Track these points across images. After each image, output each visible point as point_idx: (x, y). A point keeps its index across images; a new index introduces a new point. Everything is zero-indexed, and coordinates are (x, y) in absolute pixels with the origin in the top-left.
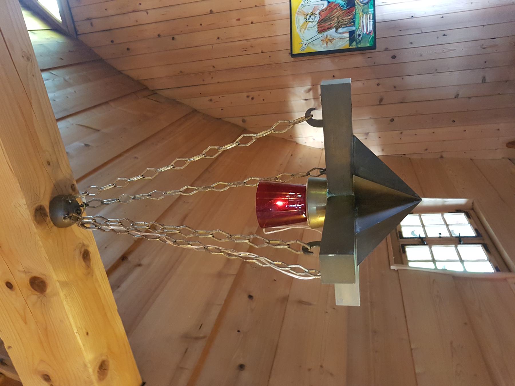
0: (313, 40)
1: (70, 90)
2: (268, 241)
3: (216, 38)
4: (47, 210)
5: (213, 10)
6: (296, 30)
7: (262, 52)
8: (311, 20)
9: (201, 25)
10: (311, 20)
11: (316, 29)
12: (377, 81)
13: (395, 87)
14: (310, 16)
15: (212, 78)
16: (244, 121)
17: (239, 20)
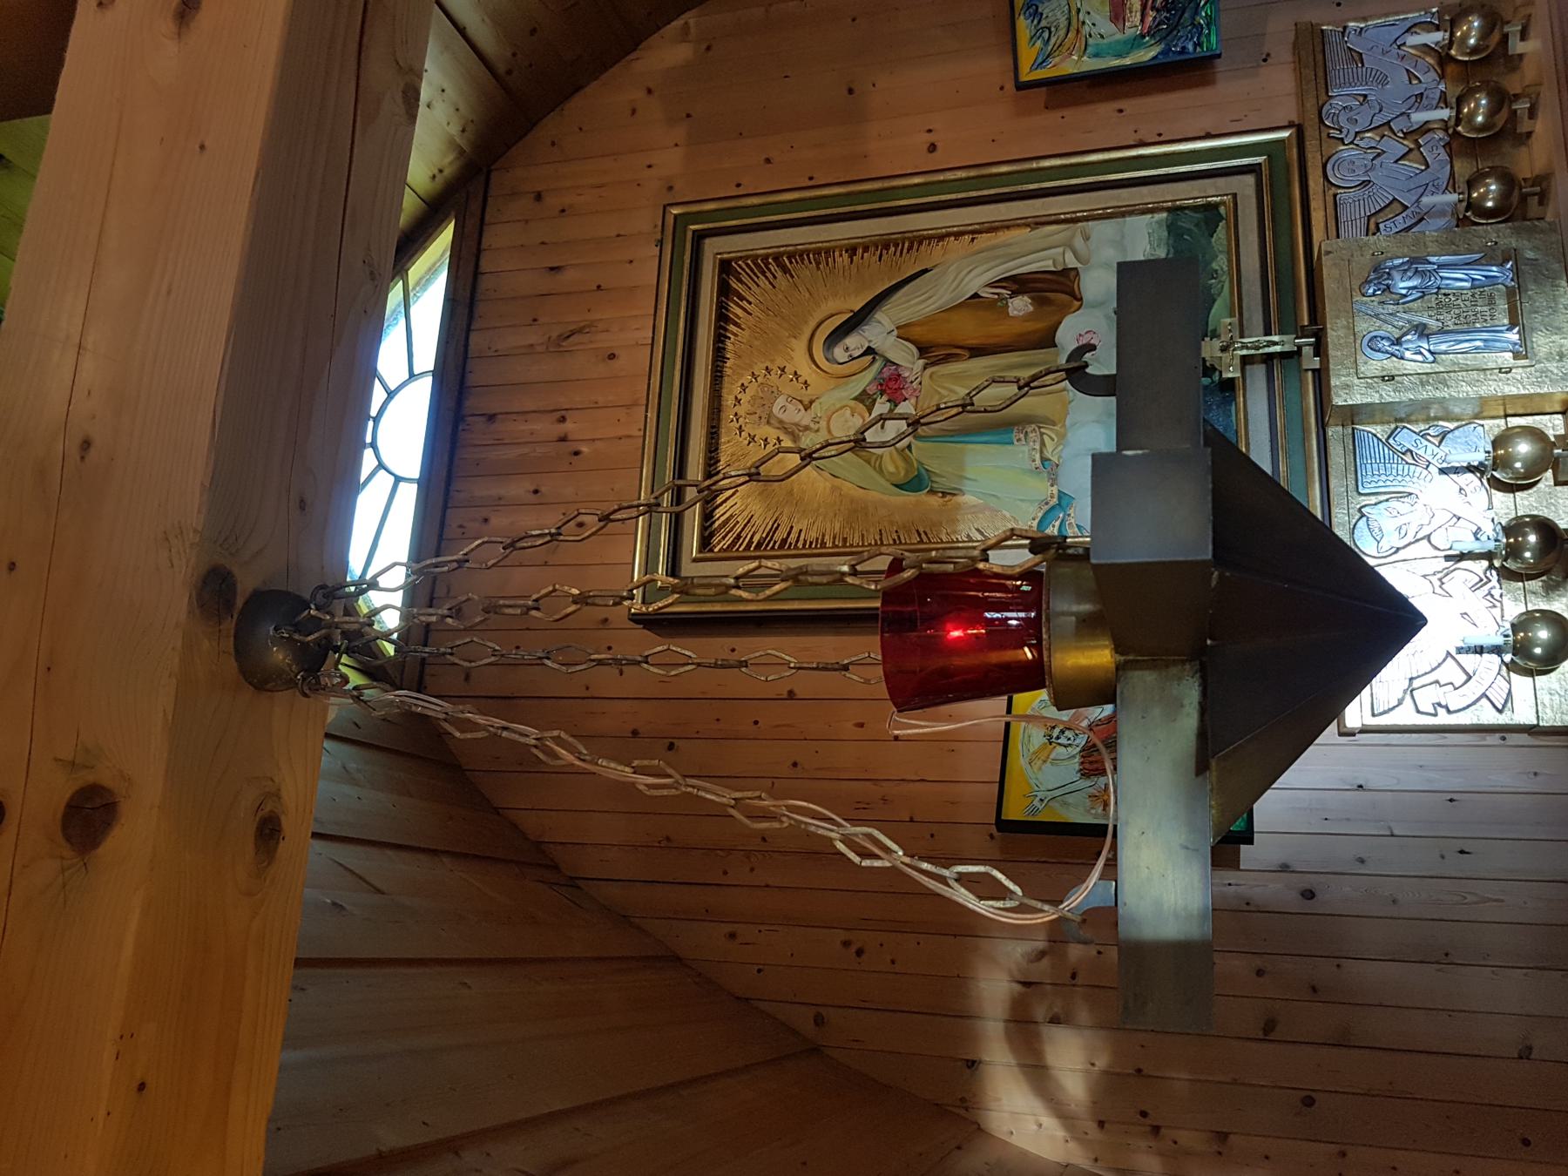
0: (1062, 794)
1: (346, 788)
2: (795, 460)
3: (789, 763)
4: (240, 602)
5: (796, 691)
6: (1018, 760)
7: (912, 820)
8: (1063, 740)
9: (756, 723)
10: (1063, 740)
11: (1075, 764)
12: (1258, 962)
13: (1314, 990)
14: (1062, 732)
15: (752, 870)
16: (819, 1021)
17: (861, 725)
